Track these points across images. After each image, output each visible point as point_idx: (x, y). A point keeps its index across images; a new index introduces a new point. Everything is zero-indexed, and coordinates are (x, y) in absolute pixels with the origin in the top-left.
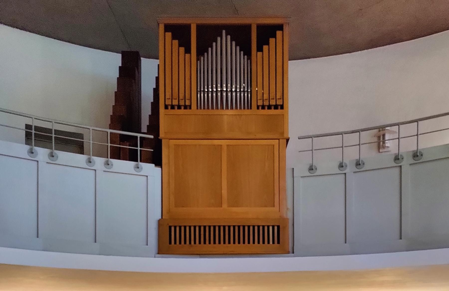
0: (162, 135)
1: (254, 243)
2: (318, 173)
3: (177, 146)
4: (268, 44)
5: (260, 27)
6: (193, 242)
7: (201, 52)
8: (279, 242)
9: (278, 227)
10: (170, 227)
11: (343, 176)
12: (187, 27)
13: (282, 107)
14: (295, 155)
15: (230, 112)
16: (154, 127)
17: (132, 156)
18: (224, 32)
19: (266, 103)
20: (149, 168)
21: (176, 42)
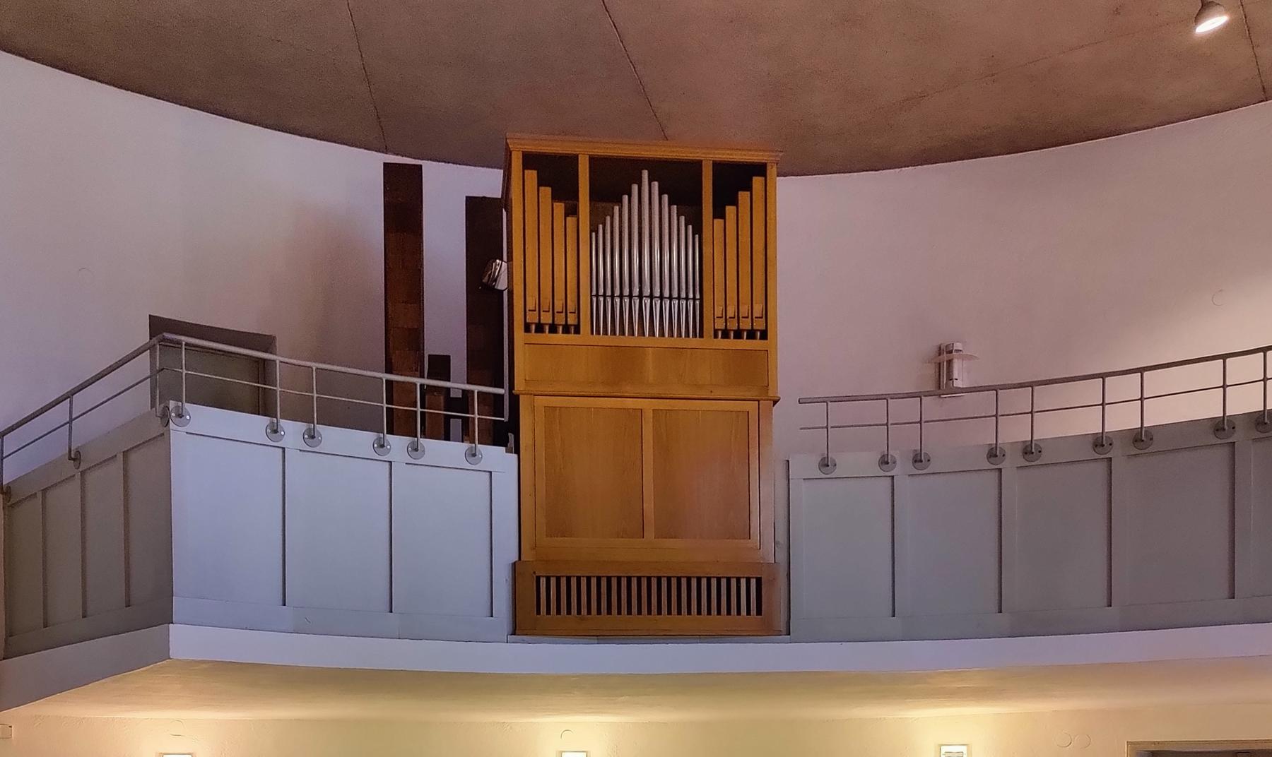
0: (519, 386)
1: (709, 613)
3: (550, 410)
5: (719, 167)
6: (584, 611)
8: (759, 612)
9: (759, 581)
10: (538, 578)
11: (889, 480)
12: (570, 161)
13: (764, 335)
14: (787, 421)
15: (657, 341)
18: (645, 174)
19: (733, 326)
20: (496, 457)
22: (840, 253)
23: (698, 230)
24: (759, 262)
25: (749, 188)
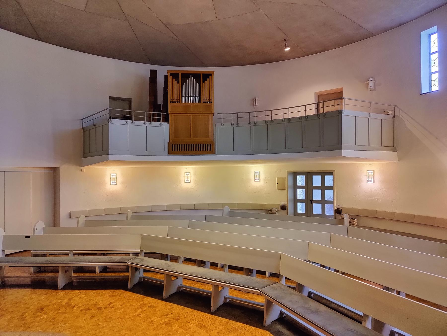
0: (169, 112)
5: (183, 75)
7: (182, 84)
13: (212, 103)
17: (158, 120)
19: (206, 101)
20: (165, 124)
22: (229, 86)
23: (200, 85)
24: (211, 91)
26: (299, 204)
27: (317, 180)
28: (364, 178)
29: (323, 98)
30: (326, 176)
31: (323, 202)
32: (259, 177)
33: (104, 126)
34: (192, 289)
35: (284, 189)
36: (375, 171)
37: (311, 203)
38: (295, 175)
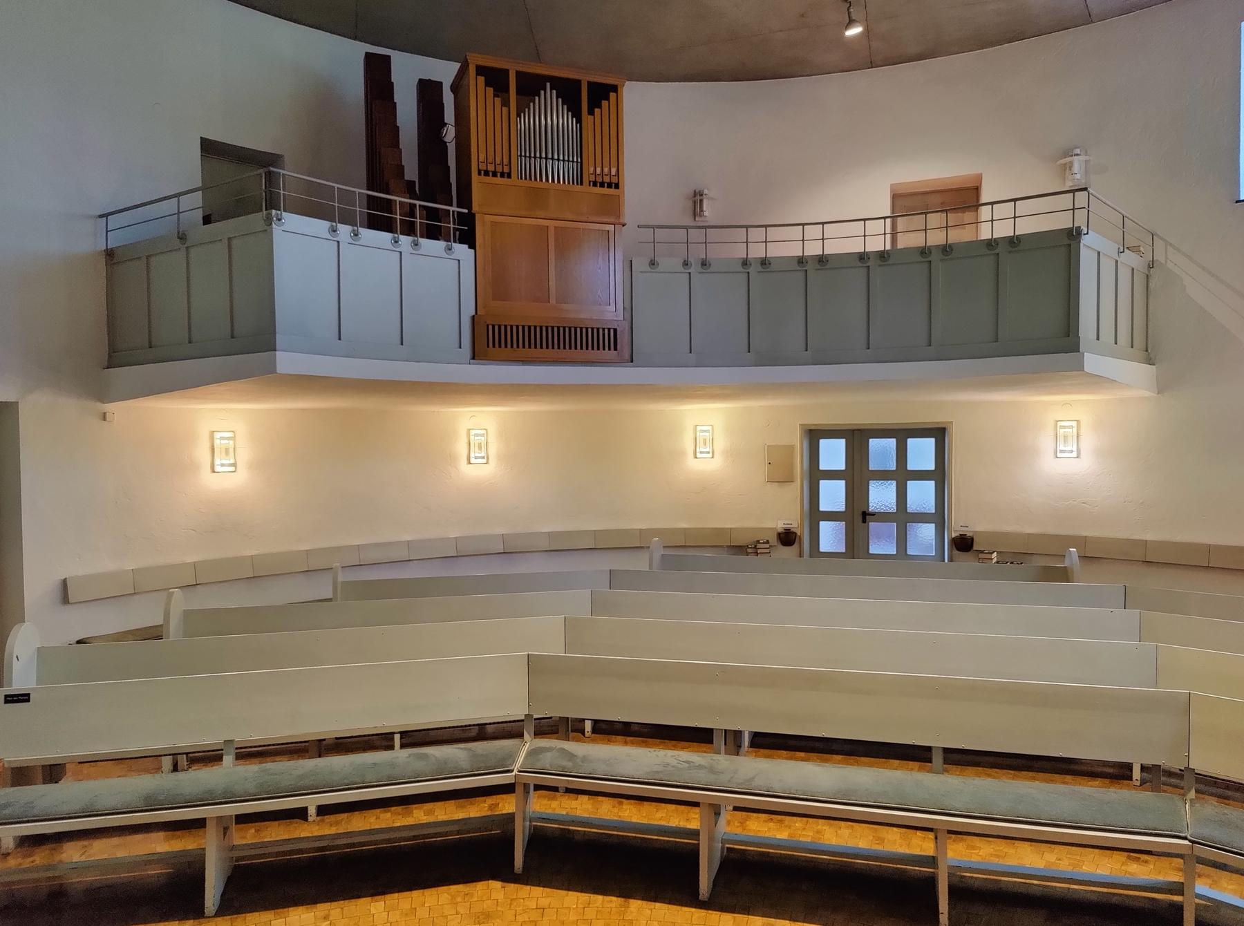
2: (660, 269)
3: (494, 224)
4: (600, 107)
9: (615, 330)
13: (617, 186)
16: (465, 198)
17: (433, 233)
18: (548, 85)
20: (462, 250)
21: (490, 90)
23: (579, 121)
25: (608, 99)
26: (825, 526)
27: (881, 451)
28: (1045, 442)
29: (908, 203)
30: (910, 441)
31: (903, 517)
32: (708, 442)
33: (234, 242)
34: (479, 830)
35: (789, 480)
36: (1083, 425)
37: (864, 521)
38: (814, 435)
